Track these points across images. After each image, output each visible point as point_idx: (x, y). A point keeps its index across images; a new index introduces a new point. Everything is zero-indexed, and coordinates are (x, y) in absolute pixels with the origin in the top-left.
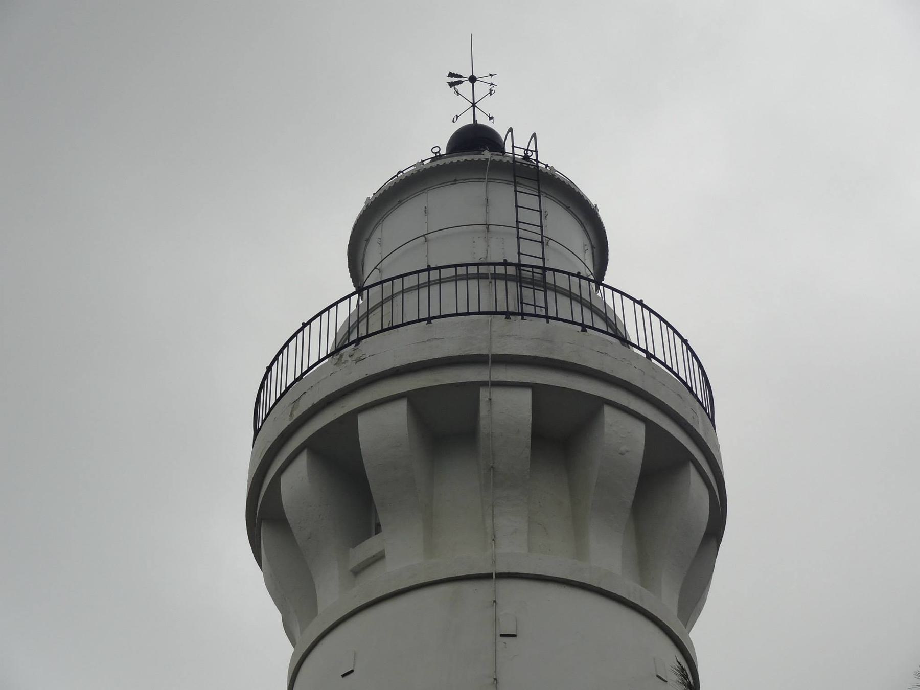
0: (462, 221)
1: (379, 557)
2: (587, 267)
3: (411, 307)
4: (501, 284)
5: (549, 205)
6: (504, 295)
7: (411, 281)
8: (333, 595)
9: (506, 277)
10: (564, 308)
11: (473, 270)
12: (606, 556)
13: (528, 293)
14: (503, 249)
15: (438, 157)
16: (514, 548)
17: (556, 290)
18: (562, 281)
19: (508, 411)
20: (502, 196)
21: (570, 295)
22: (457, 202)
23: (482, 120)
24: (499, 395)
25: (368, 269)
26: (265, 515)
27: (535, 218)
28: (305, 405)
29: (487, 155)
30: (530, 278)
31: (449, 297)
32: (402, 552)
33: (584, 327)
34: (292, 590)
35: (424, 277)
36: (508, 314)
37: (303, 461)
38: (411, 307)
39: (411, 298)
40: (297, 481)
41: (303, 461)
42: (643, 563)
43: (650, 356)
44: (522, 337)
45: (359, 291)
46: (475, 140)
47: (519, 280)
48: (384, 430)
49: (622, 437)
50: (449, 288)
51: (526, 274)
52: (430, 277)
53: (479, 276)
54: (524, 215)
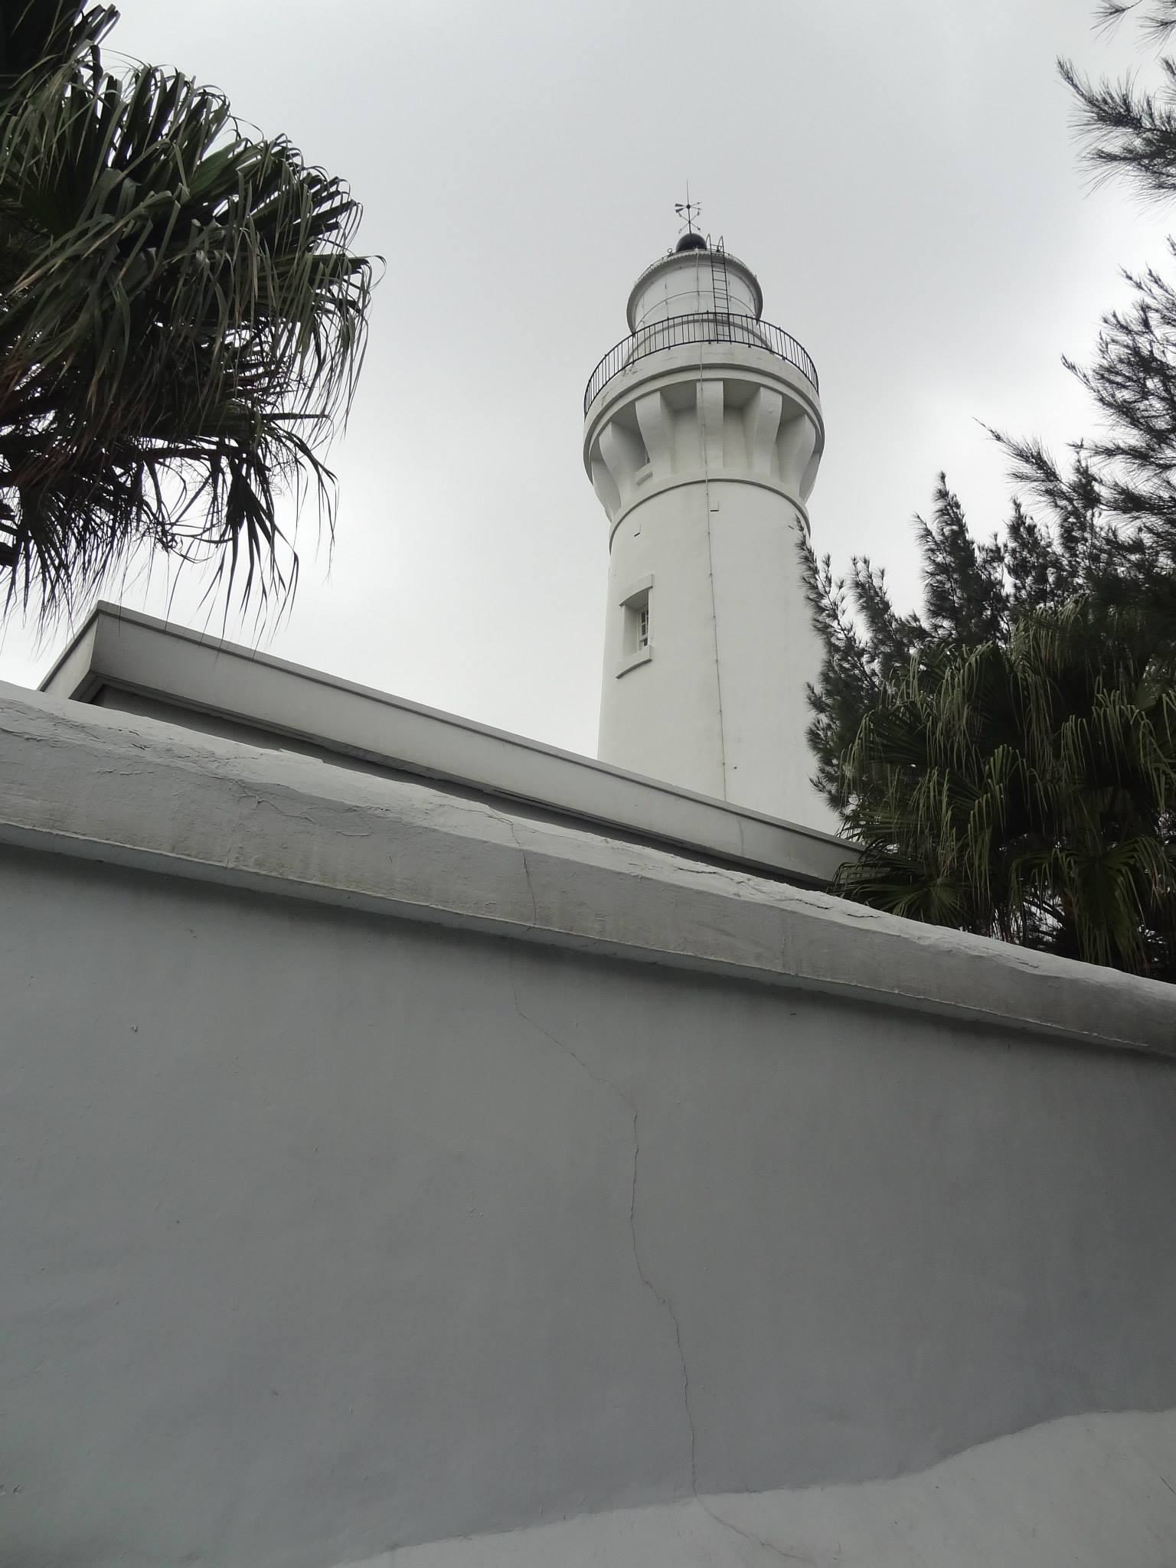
0: (689, 290)
1: (650, 475)
2: (752, 313)
3: (659, 341)
4: (706, 324)
5: (731, 278)
6: (708, 331)
7: (659, 327)
8: (629, 495)
9: (708, 321)
10: (739, 335)
11: (691, 318)
12: (763, 468)
13: (720, 328)
14: (707, 305)
15: (671, 254)
16: (716, 469)
17: (735, 325)
18: (737, 320)
19: (711, 394)
20: (705, 276)
21: (742, 328)
22: (682, 280)
23: (695, 231)
24: (706, 385)
25: (638, 319)
26: (592, 457)
27: (723, 285)
28: (609, 399)
29: (697, 251)
30: (721, 320)
31: (678, 334)
32: (661, 472)
33: (750, 345)
34: (609, 495)
35: (666, 324)
36: (710, 341)
37: (610, 427)
38: (659, 341)
39: (659, 337)
40: (608, 439)
41: (610, 427)
42: (781, 470)
43: (784, 358)
44: (717, 353)
45: (633, 335)
46: (691, 242)
47: (715, 321)
48: (649, 409)
49: (770, 403)
50: (678, 329)
51: (719, 318)
52: (669, 323)
53: (694, 321)
54: (717, 284)
